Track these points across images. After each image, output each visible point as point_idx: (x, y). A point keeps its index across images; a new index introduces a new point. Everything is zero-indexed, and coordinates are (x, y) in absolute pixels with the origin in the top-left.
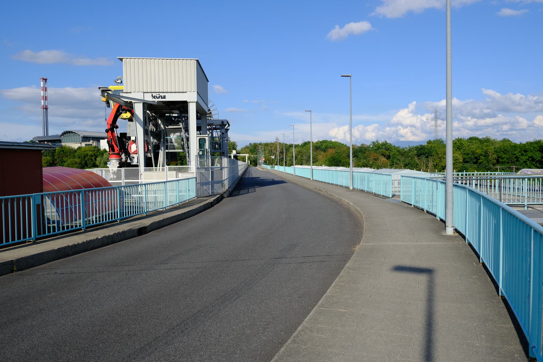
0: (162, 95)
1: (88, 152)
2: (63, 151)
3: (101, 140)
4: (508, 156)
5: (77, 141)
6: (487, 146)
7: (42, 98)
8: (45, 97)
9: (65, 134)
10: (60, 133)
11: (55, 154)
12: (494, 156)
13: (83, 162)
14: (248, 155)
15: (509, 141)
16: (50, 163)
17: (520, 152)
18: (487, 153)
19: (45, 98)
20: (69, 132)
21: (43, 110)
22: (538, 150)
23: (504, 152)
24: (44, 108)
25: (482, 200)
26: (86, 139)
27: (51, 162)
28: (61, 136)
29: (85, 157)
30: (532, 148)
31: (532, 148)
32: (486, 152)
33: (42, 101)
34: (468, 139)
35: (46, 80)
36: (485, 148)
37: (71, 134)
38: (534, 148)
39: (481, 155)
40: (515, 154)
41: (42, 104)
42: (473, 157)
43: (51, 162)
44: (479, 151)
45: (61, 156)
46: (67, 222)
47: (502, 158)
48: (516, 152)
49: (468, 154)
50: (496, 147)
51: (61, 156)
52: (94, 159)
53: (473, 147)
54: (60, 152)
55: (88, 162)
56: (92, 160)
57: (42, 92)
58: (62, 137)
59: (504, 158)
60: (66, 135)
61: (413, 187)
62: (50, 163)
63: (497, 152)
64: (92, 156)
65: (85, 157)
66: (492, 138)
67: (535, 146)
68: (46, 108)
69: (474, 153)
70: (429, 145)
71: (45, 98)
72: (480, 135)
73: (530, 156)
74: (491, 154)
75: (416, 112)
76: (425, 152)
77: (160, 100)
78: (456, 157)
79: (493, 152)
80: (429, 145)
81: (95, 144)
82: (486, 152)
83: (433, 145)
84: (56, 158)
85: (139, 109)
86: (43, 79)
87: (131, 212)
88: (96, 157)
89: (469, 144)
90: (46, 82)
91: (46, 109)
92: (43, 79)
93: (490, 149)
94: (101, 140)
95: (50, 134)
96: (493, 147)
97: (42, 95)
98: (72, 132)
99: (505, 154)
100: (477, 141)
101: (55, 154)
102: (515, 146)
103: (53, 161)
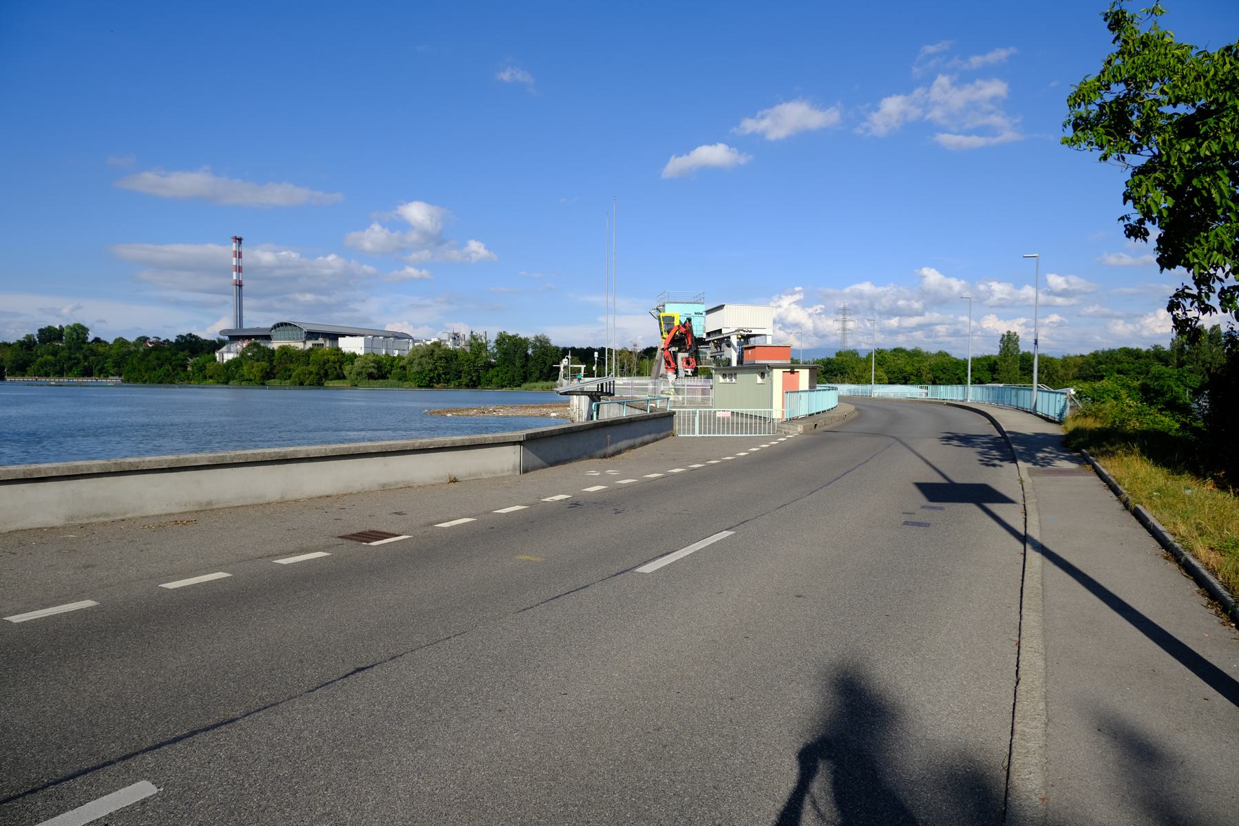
0: (750, 330)
1: (329, 356)
2: (286, 353)
3: (339, 338)
4: (949, 377)
5: (298, 339)
6: (919, 362)
7: (234, 268)
8: (239, 267)
9: (278, 327)
10: (270, 325)
11: (273, 358)
12: (928, 375)
13: (322, 372)
14: (585, 366)
15: (947, 355)
16: (266, 372)
17: (963, 371)
18: (920, 372)
19: (239, 269)
20: (286, 324)
21: (235, 287)
22: (988, 370)
23: (942, 371)
24: (237, 285)
25: (604, 487)
26: (312, 335)
27: (268, 370)
28: (272, 329)
29: (325, 363)
30: (980, 366)
31: (980, 366)
32: (919, 370)
33: (234, 273)
34: (891, 352)
35: (240, 240)
36: (917, 365)
37: (289, 327)
38: (983, 366)
39: (912, 374)
40: (957, 374)
41: (235, 278)
42: (900, 377)
43: (268, 370)
44: (909, 369)
45: (283, 361)
46: (751, 424)
47: (939, 380)
48: (958, 372)
49: (894, 373)
50: (932, 363)
51: (283, 361)
52: (338, 367)
53: (901, 362)
54: (282, 355)
55: (329, 371)
56: (336, 369)
57: (234, 259)
58: (273, 331)
59: (943, 379)
60: (281, 328)
61: (507, 434)
62: (266, 372)
63: (933, 371)
64: (334, 362)
65: (325, 363)
66: (925, 349)
67: (984, 363)
68: (240, 285)
69: (901, 371)
70: (840, 358)
71: (239, 269)
72: (903, 342)
73: (977, 377)
74: (924, 373)
75: (802, 304)
76: (833, 368)
77: (748, 333)
78: (881, 376)
79: (928, 371)
80: (840, 358)
81: (328, 344)
82: (919, 370)
83: (845, 359)
84: (274, 364)
85: (734, 340)
86: (236, 239)
87: (710, 424)
88: (342, 363)
89: (893, 358)
90: (240, 243)
91: (240, 286)
92: (236, 239)
93: (924, 366)
94: (339, 338)
95: (245, 326)
96: (928, 363)
97: (234, 263)
98: (290, 325)
99: (944, 373)
100: (903, 354)
101: (273, 358)
102: (957, 363)
103: (271, 369)
